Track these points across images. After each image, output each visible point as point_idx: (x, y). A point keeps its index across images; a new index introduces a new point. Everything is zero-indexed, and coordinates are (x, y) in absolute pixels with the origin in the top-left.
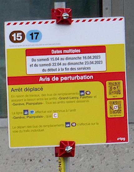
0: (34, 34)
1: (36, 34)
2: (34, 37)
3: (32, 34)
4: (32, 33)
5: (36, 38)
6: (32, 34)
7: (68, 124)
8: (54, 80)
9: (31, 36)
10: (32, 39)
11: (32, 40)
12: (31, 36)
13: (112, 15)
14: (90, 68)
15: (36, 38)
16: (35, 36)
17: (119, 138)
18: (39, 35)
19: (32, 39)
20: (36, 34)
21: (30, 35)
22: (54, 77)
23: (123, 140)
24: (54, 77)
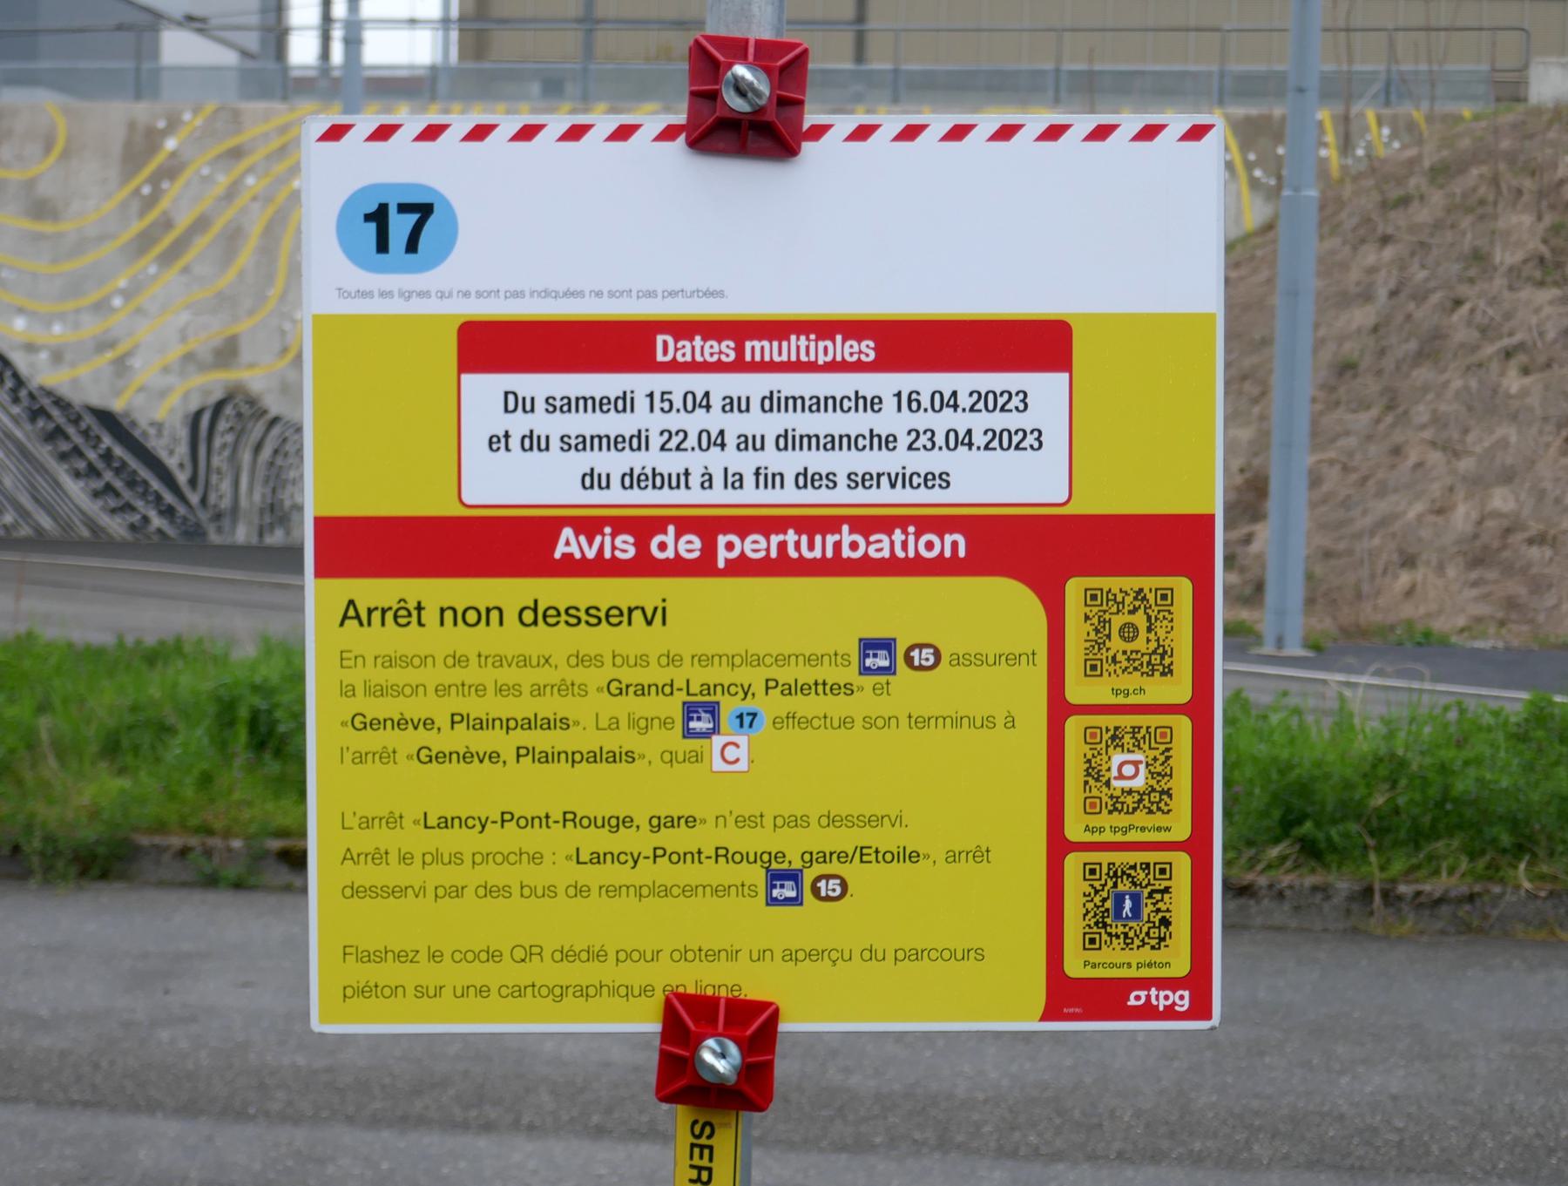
0: (393, 210)
1: (413, 218)
9: (372, 226)
12: (372, 226)
17: (1143, 994)
20: (413, 218)
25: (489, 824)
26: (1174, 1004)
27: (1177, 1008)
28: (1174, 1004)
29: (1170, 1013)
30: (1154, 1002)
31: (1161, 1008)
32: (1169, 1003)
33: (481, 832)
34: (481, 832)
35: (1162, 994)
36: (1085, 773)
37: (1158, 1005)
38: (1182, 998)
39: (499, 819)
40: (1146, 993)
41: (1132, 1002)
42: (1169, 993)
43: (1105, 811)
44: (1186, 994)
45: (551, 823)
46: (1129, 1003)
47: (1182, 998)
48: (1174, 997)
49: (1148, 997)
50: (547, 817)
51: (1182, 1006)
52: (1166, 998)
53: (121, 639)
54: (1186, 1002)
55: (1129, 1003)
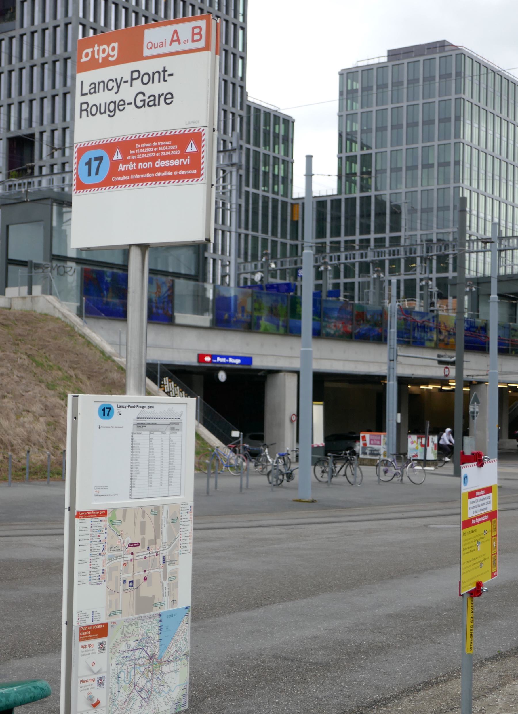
0: (93, 160)
1: (98, 162)
2: (106, 414)
3: (104, 410)
4: (104, 408)
5: (108, 415)
6: (104, 410)
7: (48, 172)
8: (159, 166)
9: (87, 166)
10: (104, 415)
11: (89, 177)
12: (87, 166)
13: (392, 55)
14: (486, 509)
15: (108, 415)
16: (107, 411)
17: (89, 51)
18: (103, 162)
19: (104, 415)
20: (98, 162)
21: (102, 410)
22: (159, 160)
23: (105, 59)
24: (159, 160)
25: (123, 85)
26: (109, 55)
27: (111, 59)
28: (109, 55)
29: (106, 63)
30: (96, 56)
31: (100, 61)
32: (104, 55)
33: (116, 93)
34: (116, 93)
35: (101, 48)
36: (461, 597)
37: (98, 59)
38: (113, 49)
39: (129, 79)
40: (91, 49)
41: (84, 59)
42: (105, 46)
43: (91, 570)
44: (116, 45)
45: (167, 78)
46: (82, 61)
47: (113, 49)
48: (108, 50)
49: (93, 52)
50: (165, 71)
51: (113, 56)
52: (104, 51)
53: (48, 483)
54: (116, 52)
55: (82, 61)
